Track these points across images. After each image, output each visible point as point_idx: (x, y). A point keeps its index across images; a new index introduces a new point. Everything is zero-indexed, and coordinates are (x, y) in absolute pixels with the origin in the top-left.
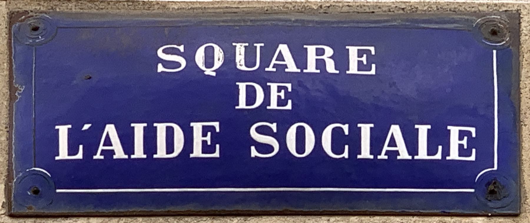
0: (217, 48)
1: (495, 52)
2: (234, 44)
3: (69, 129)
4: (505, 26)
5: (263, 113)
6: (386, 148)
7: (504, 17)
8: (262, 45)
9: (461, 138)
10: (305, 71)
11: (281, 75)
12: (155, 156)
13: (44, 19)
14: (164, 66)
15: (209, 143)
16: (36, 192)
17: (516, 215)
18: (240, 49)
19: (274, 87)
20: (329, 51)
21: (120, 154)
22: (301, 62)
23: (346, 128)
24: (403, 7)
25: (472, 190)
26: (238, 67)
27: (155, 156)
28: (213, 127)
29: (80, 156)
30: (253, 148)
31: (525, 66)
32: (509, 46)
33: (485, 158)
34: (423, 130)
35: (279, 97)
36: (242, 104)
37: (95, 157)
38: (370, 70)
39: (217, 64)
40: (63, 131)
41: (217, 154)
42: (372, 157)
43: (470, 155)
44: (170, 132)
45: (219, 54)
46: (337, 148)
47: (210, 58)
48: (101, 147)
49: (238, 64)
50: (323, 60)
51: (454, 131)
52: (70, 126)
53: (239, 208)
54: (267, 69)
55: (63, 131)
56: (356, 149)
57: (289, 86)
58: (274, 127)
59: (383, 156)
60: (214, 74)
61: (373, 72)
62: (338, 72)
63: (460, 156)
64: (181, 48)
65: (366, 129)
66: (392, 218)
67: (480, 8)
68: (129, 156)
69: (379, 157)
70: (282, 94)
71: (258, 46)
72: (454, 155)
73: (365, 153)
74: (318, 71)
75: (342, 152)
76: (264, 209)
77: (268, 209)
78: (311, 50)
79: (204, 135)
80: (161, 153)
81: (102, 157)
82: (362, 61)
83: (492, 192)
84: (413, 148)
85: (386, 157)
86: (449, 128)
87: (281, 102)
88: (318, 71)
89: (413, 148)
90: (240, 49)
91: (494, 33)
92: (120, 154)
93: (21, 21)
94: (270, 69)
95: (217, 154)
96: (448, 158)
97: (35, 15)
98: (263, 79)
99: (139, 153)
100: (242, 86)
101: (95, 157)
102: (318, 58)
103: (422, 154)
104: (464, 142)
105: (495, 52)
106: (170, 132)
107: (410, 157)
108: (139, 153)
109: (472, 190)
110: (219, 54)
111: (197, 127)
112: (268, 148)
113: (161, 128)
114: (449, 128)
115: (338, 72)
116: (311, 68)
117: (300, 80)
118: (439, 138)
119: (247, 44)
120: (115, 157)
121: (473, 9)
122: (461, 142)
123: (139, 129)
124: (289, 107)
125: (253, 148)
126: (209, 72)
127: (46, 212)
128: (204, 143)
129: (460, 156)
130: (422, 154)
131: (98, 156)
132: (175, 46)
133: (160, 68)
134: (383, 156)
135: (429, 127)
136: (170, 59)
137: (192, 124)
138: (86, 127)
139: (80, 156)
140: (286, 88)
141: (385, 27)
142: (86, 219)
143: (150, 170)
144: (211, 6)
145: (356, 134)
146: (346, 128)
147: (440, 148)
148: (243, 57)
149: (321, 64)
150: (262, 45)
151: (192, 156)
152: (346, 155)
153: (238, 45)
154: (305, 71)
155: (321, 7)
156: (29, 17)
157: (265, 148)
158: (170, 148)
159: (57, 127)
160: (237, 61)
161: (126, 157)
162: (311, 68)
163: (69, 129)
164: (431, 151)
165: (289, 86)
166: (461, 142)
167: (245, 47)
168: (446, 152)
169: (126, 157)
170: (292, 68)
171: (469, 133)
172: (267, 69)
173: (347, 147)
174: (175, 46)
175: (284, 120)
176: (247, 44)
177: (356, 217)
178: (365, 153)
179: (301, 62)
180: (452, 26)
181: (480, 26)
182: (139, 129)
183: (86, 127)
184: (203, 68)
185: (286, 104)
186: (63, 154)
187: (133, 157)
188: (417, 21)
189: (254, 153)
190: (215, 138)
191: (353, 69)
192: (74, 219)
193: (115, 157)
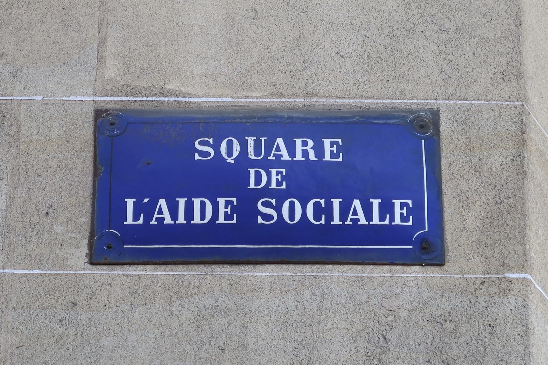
0: (235, 142)
1: (423, 141)
2: (246, 138)
3: (134, 201)
4: (429, 121)
5: (266, 192)
6: (350, 216)
7: (428, 113)
8: (266, 138)
9: (402, 208)
10: (294, 159)
11: (278, 162)
12: (192, 222)
13: (117, 116)
14: (200, 155)
15: (229, 213)
16: (109, 247)
17: (442, 265)
18: (251, 141)
19: (274, 171)
20: (311, 143)
21: (168, 220)
22: (292, 151)
23: (323, 202)
24: (360, 106)
25: (411, 247)
26: (250, 156)
27: (192, 222)
28: (233, 202)
29: (141, 222)
30: (259, 217)
31: (444, 150)
32: (432, 136)
33: (419, 223)
34: (376, 203)
35: (277, 179)
36: (252, 185)
37: (151, 223)
38: (339, 158)
39: (236, 154)
40: (130, 203)
41: (234, 221)
42: (341, 223)
43: (408, 221)
44: (203, 204)
45: (236, 146)
46: (317, 217)
47: (229, 150)
48: (156, 215)
49: (249, 154)
50: (307, 150)
51: (397, 203)
52: (135, 200)
53: (250, 259)
54: (269, 158)
55: (130, 203)
56: (330, 217)
57: (284, 171)
58: (274, 201)
59: (348, 223)
60: (233, 162)
61: (341, 159)
62: (317, 159)
63: (401, 222)
64: (211, 141)
65: (336, 203)
66: (356, 266)
67: (412, 106)
68: (175, 222)
69: (346, 223)
70: (279, 177)
71: (263, 139)
72: (397, 221)
73: (336, 220)
74: (304, 159)
75: (321, 220)
76: (267, 260)
77: (270, 259)
78: (299, 142)
79: (226, 207)
80: (197, 220)
81: (156, 223)
82: (333, 151)
83: (425, 248)
84: (369, 217)
85: (351, 223)
86: (393, 201)
87: (279, 183)
88: (304, 159)
89: (369, 217)
90: (251, 141)
91: (422, 126)
92: (168, 220)
93: (103, 117)
94: (271, 158)
95: (234, 221)
96: (393, 223)
97: (112, 112)
98: (266, 165)
99: (181, 220)
100: (252, 171)
101: (151, 223)
102: (304, 148)
103: (376, 221)
104: (404, 211)
105: (423, 141)
106: (203, 204)
107: (367, 223)
108: (181, 220)
109: (411, 247)
110: (236, 146)
111: (221, 201)
112: (270, 217)
113: (197, 202)
114: (393, 201)
115: (317, 159)
116: (299, 157)
117: (291, 165)
118: (387, 209)
119: (255, 138)
120: (165, 223)
121: (408, 107)
122: (402, 211)
123: (182, 202)
124: (284, 187)
125: (259, 217)
126: (230, 160)
127: (117, 262)
128: (226, 213)
129: (401, 222)
130: (376, 221)
131: (153, 222)
132: (207, 139)
133: (197, 157)
134: (348, 223)
135: (380, 200)
136: (203, 149)
137: (218, 199)
138: (146, 200)
139: (141, 222)
140: (282, 173)
141: (346, 123)
142: (143, 266)
143: (189, 232)
144: (230, 105)
145: (330, 206)
146: (323, 202)
147: (388, 216)
148: (252, 148)
149: (305, 153)
150: (266, 138)
151: (217, 222)
152: (323, 221)
153: (249, 139)
154: (294, 159)
155: (305, 105)
156: (109, 114)
157: (267, 217)
158: (203, 217)
159: (126, 200)
160: (249, 151)
161: (173, 222)
162: (299, 157)
163: (134, 201)
164: (382, 218)
165: (284, 171)
166: (402, 211)
167: (254, 140)
168: (392, 219)
169: (173, 222)
170: (286, 157)
171: (407, 204)
172: (269, 158)
173: (323, 216)
174: (207, 139)
175: (281, 196)
176: (255, 138)
177: (331, 266)
178: (336, 220)
179: (292, 151)
180: (393, 121)
181: (412, 121)
182: (182, 202)
183: (146, 200)
184: (226, 157)
185: (282, 185)
186: (130, 220)
187: (177, 222)
188: (369, 118)
189: (260, 220)
190: (234, 209)
191: (327, 157)
192: (136, 266)
193: (165, 223)
